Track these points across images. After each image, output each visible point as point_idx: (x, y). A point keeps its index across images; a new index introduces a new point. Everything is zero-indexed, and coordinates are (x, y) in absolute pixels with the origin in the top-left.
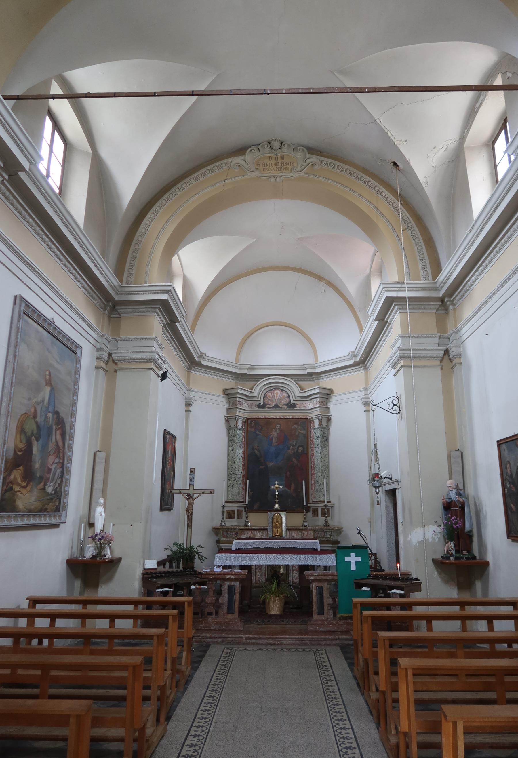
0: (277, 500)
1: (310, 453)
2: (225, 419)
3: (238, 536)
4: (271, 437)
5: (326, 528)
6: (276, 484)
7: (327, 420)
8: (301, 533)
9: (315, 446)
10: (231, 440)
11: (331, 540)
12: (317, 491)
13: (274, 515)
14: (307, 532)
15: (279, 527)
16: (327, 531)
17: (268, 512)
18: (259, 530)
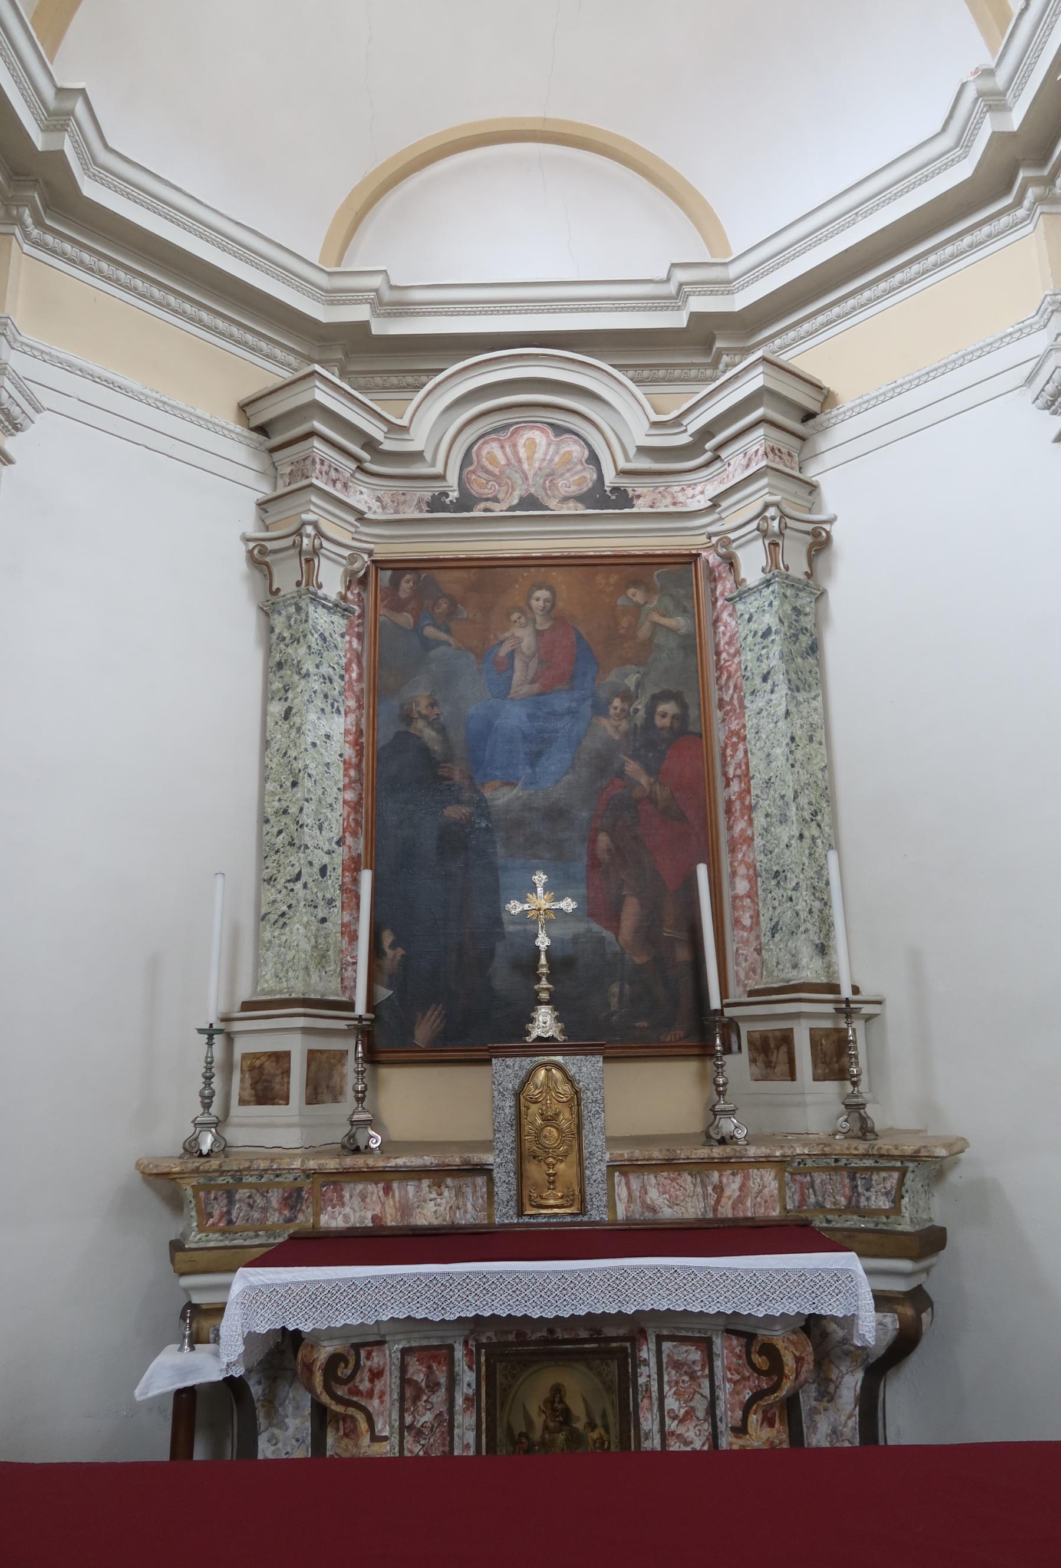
0: (544, 984)
1: (719, 735)
2: (250, 552)
3: (301, 1217)
4: (504, 651)
5: (862, 1147)
6: (533, 888)
7: (812, 545)
8: (704, 1186)
9: (747, 687)
10: (280, 665)
11: (906, 1227)
12: (774, 930)
13: (530, 1074)
14: (738, 1179)
15: (565, 1155)
16: (867, 1169)
17: (487, 1062)
18: (437, 1175)
